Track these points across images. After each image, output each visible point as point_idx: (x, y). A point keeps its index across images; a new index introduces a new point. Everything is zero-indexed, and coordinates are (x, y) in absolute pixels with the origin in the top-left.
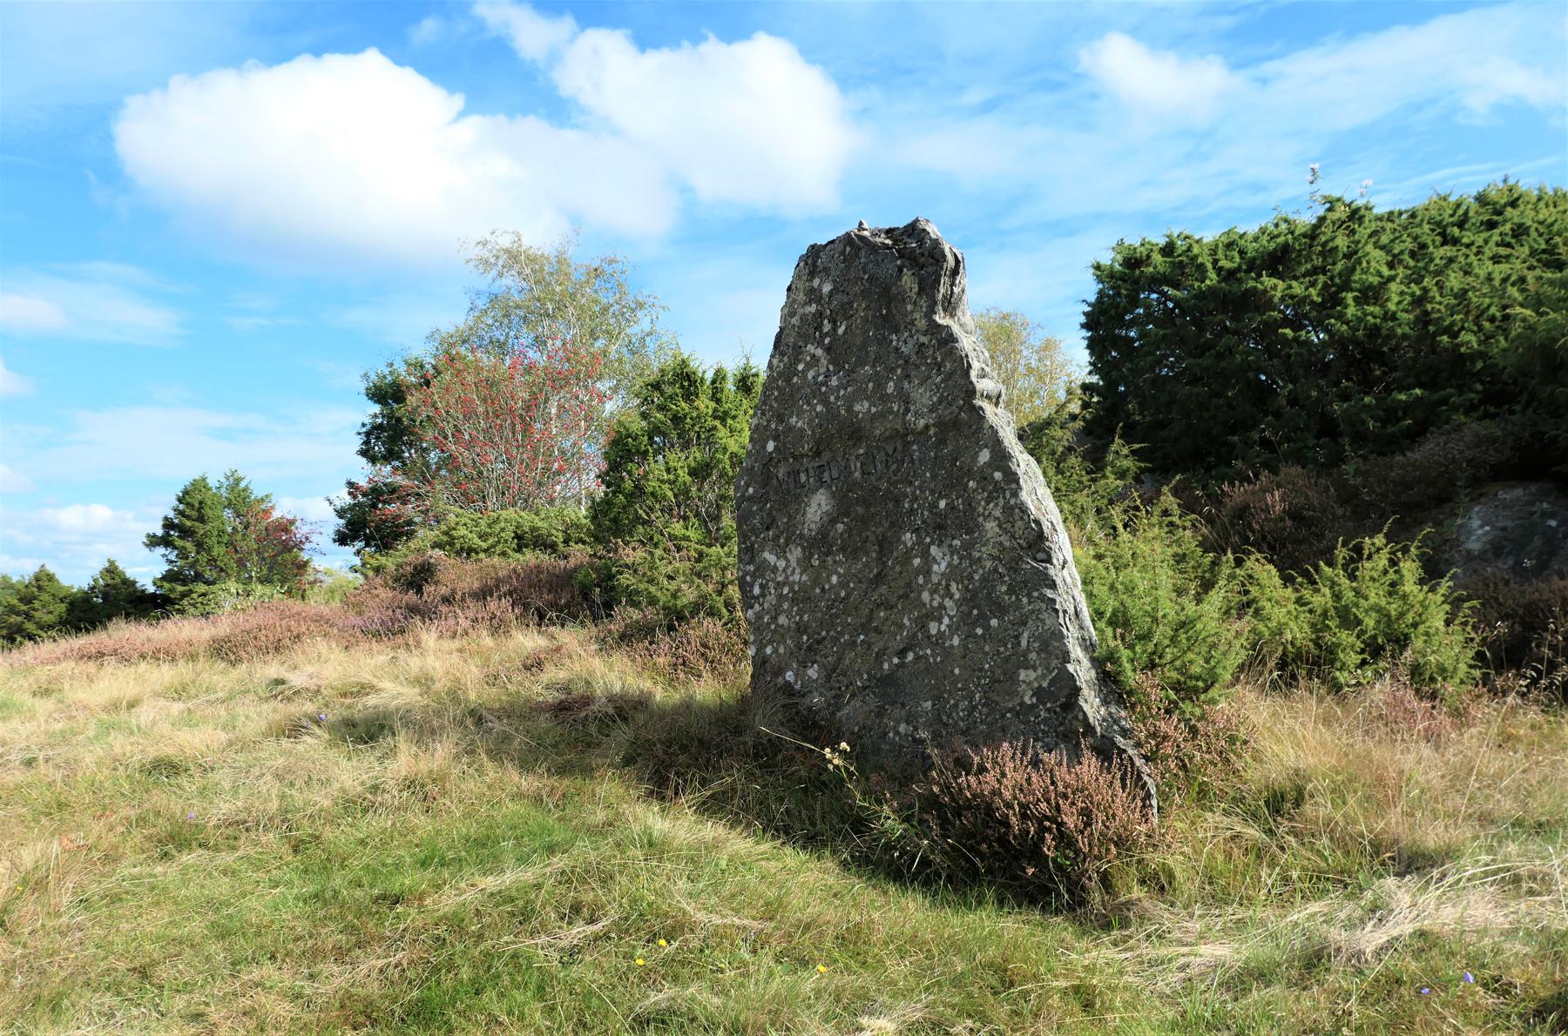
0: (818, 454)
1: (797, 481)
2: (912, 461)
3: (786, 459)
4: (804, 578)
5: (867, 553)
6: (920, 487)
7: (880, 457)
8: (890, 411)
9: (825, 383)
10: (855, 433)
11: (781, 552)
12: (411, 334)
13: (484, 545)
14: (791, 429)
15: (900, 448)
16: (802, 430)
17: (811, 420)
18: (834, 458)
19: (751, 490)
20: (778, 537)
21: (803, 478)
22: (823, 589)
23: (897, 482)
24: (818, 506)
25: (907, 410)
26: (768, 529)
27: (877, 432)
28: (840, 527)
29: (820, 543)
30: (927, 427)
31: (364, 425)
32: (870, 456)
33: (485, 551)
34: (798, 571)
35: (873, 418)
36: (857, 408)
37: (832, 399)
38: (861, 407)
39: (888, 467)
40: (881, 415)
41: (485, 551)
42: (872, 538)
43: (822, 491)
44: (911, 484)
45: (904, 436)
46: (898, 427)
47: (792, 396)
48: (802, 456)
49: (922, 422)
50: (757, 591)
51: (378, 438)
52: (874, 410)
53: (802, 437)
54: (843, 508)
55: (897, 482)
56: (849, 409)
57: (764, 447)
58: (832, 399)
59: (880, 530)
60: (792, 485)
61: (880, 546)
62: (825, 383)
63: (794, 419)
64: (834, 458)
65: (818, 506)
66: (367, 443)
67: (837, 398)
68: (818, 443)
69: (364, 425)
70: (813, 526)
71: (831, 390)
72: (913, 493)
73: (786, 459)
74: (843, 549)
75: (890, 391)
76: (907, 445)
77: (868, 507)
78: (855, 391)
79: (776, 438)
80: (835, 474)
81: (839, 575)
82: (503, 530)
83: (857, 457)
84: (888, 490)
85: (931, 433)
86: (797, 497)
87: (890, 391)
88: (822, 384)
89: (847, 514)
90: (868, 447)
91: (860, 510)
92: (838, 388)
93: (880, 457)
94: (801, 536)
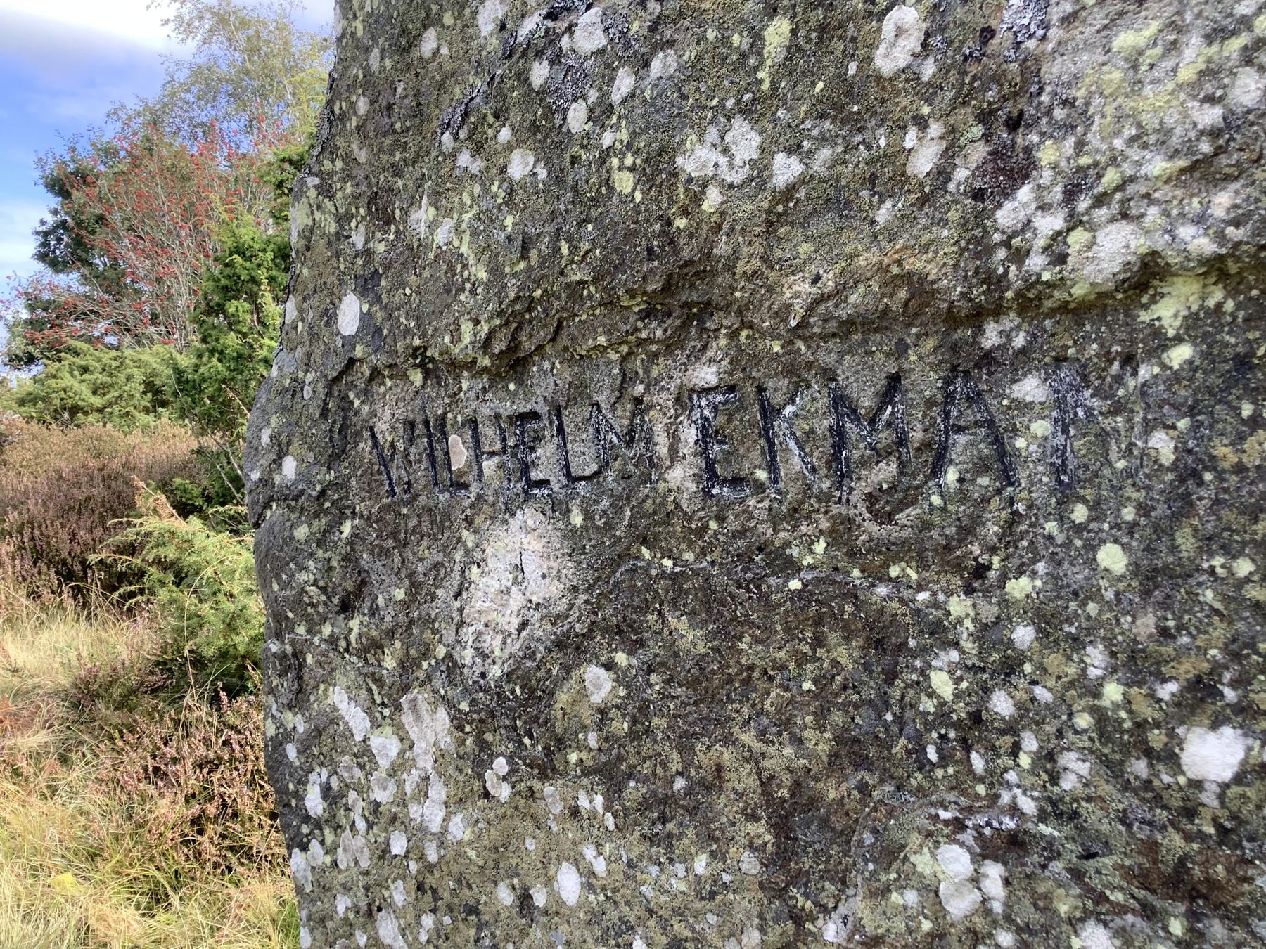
0: (513, 365)
1: (438, 460)
2: (1002, 463)
3: (400, 374)
4: (459, 829)
5: (715, 842)
6: (1046, 619)
7: (807, 411)
8: (887, 175)
9: (545, 47)
10: (682, 292)
11: (387, 701)
12: (89, 120)
13: (97, 401)
14: (413, 252)
15: (924, 380)
16: (453, 260)
17: (489, 219)
18: (579, 390)
19: (290, 467)
20: (377, 646)
21: (460, 454)
22: (524, 899)
23: (893, 551)
24: (514, 575)
25: (1010, 170)
26: (346, 607)
27: (797, 291)
28: (599, 684)
29: (512, 715)
30: (1147, 275)
31: (43, 223)
32: (745, 409)
33: (100, 410)
34: (438, 792)
35: (782, 212)
36: (697, 158)
37: (577, 117)
38: (719, 157)
39: (840, 468)
40: (835, 199)
41: (100, 410)
42: (743, 779)
43: (528, 516)
44: (975, 578)
45: (968, 323)
46: (929, 267)
47: (418, 112)
48: (456, 366)
49: (1110, 249)
50: (314, 803)
51: (59, 240)
52: (786, 169)
53: (452, 289)
54: (613, 606)
55: (893, 551)
56: (657, 167)
57: (329, 317)
58: (577, 117)
59: (781, 756)
60: (421, 473)
61: (781, 827)
62: (545, 47)
63: (423, 215)
64: (579, 390)
65: (514, 575)
66: (45, 244)
67: (601, 114)
68: (516, 317)
69: (43, 223)
70: (493, 643)
71: (575, 73)
72: (988, 633)
73: (400, 374)
74: (609, 775)
75: (892, 56)
76: (971, 371)
77: (726, 633)
78: (695, 71)
79: (367, 286)
80: (584, 461)
81: (588, 876)
82: (129, 378)
83: (685, 398)
84: (831, 577)
85: (1167, 312)
86: (440, 520)
87: (892, 56)
88: (533, 51)
89: (628, 634)
90: (740, 360)
91: (690, 636)
92: (607, 61)
93: (807, 411)
94: (452, 667)
